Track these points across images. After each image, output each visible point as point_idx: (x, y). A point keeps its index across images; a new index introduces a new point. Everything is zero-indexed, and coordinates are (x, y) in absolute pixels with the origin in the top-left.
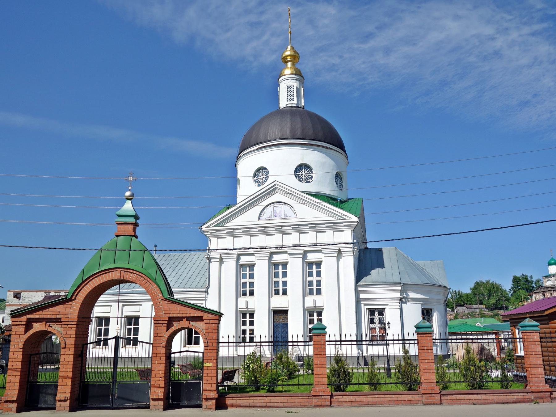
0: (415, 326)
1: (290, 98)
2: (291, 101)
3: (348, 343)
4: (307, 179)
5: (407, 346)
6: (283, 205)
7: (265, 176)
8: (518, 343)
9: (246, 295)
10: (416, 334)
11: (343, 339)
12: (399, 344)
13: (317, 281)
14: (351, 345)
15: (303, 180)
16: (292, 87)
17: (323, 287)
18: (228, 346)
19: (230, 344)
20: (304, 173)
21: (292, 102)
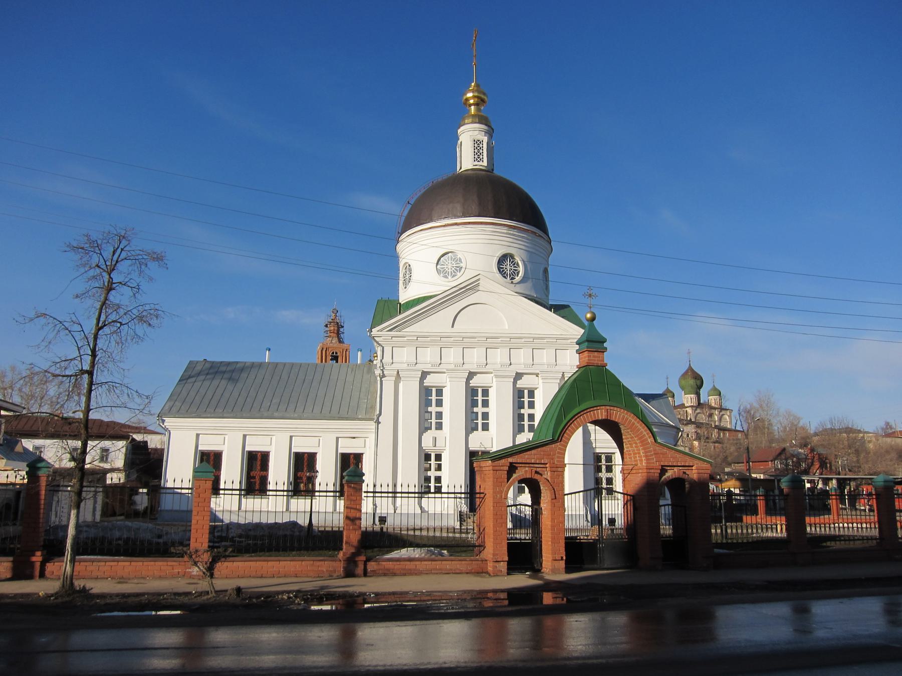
1: (478, 156)
2: (479, 161)
3: (383, 495)
4: (512, 275)
5: (398, 500)
7: (446, 266)
9: (478, 430)
11: (399, 490)
12: (388, 497)
13: (483, 413)
14: (408, 497)
16: (480, 142)
17: (446, 421)
18: (435, 498)
20: (508, 267)
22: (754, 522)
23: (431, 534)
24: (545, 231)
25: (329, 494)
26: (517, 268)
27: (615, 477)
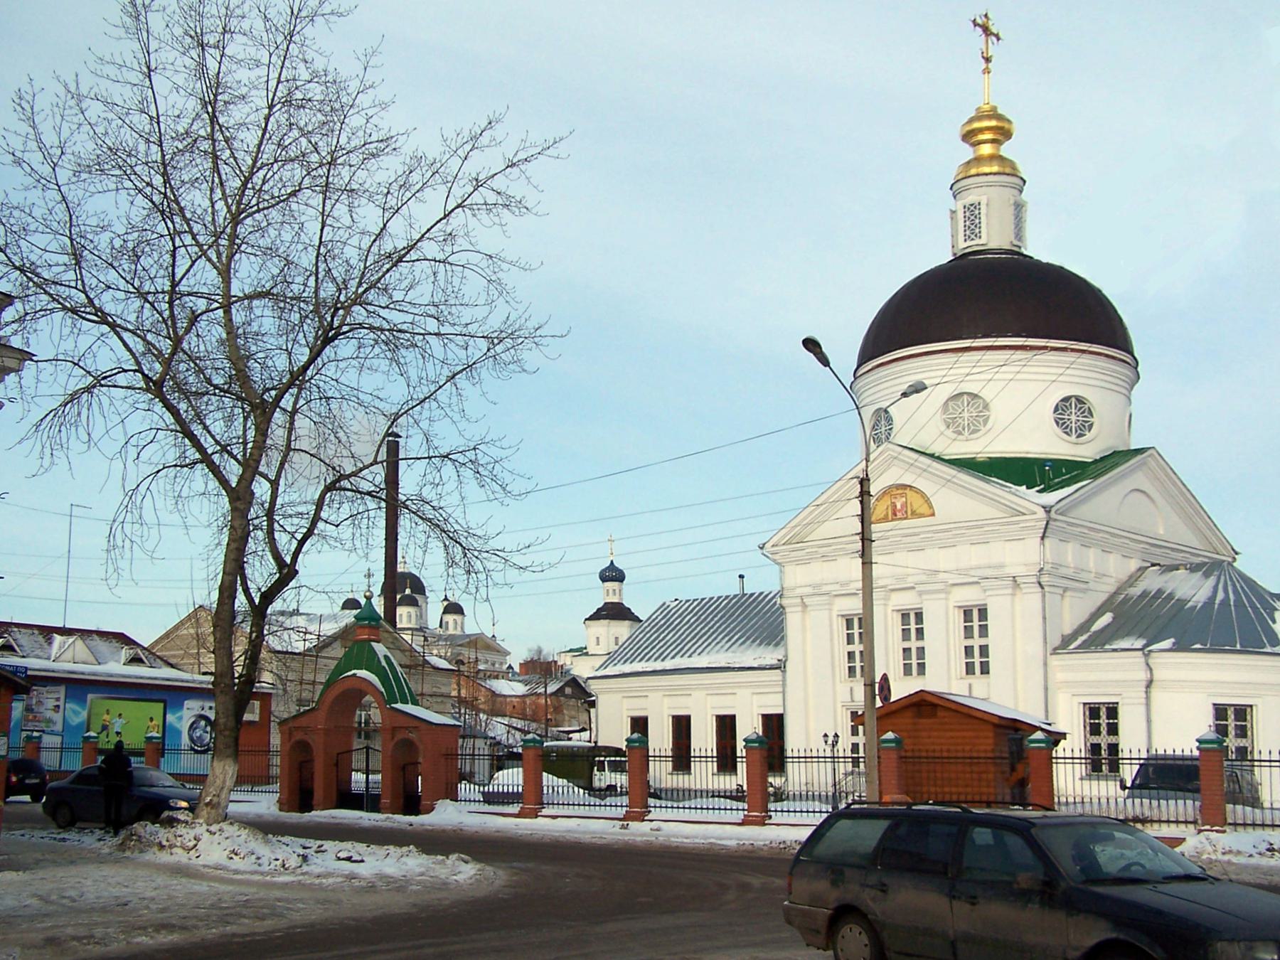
0: (1198, 740)
2: (973, 239)
3: (795, 760)
6: (908, 491)
8: (459, 761)
10: (744, 751)
11: (836, 755)
14: (1270, 766)
15: (1071, 430)
19: (1273, 764)
21: (977, 241)
22: (1103, 793)
23: (1079, 810)
24: (1125, 346)
25: (827, 760)
26: (1059, 418)
27: (1085, 736)
